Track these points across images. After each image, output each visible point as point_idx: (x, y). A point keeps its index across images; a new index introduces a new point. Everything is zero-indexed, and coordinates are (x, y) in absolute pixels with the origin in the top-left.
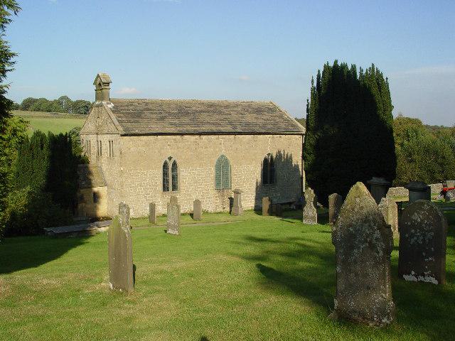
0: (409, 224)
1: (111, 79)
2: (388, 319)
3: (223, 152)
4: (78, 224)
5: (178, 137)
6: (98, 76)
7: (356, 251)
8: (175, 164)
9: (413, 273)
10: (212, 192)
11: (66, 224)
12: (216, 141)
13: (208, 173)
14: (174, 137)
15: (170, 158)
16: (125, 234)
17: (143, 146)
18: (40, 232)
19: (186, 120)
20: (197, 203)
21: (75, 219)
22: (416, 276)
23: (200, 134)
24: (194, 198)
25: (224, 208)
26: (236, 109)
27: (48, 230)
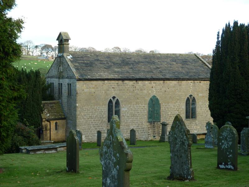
0: (222, 137)
1: (71, 36)
2: (190, 177)
3: (154, 93)
4: (59, 118)
5: (120, 82)
6: (60, 34)
7: (177, 146)
8: (117, 103)
9: (223, 163)
10: (146, 125)
11: (38, 144)
12: (149, 85)
13: (143, 110)
14: (117, 82)
15: (114, 98)
16: (75, 140)
17: (93, 88)
18: (18, 151)
19: (126, 68)
20: (133, 132)
21: (42, 142)
22: (225, 165)
23: (137, 80)
24: (132, 127)
25: (154, 137)
26: (166, 60)
27: (23, 148)
